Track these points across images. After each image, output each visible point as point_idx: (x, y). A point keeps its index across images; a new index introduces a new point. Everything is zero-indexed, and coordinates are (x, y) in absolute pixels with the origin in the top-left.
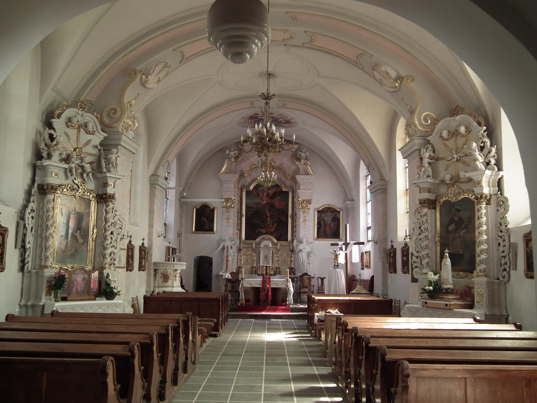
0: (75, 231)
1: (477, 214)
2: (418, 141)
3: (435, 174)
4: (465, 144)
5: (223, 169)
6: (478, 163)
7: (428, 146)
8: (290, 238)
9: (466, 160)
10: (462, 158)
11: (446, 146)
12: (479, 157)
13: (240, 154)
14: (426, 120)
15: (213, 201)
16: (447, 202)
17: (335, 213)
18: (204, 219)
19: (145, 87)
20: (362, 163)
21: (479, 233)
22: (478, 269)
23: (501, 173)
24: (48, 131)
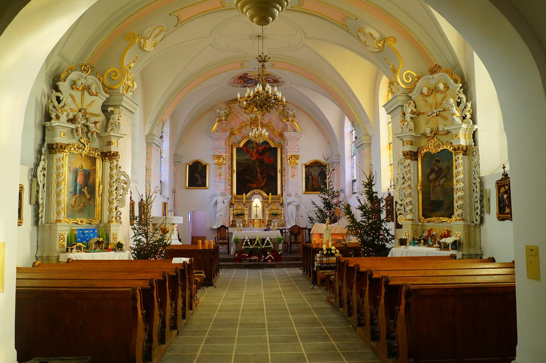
0: (82, 187)
1: (454, 164)
2: (401, 99)
3: (416, 126)
4: (443, 100)
5: (215, 127)
6: (455, 117)
7: (410, 101)
8: (279, 192)
9: (442, 113)
10: (441, 113)
11: (426, 101)
12: (456, 112)
13: (230, 114)
14: (407, 79)
15: (205, 158)
16: (428, 153)
17: (322, 167)
18: (197, 175)
19: (144, 50)
20: (346, 119)
21: (457, 181)
22: (456, 213)
23: (476, 127)
24: (55, 94)
